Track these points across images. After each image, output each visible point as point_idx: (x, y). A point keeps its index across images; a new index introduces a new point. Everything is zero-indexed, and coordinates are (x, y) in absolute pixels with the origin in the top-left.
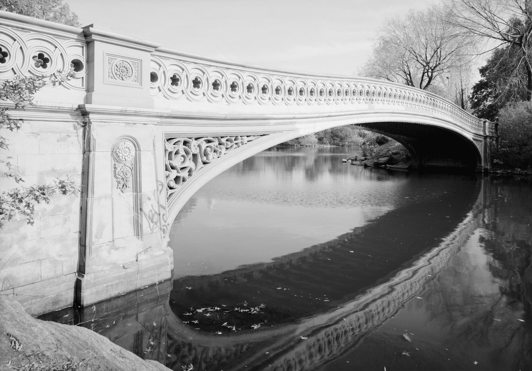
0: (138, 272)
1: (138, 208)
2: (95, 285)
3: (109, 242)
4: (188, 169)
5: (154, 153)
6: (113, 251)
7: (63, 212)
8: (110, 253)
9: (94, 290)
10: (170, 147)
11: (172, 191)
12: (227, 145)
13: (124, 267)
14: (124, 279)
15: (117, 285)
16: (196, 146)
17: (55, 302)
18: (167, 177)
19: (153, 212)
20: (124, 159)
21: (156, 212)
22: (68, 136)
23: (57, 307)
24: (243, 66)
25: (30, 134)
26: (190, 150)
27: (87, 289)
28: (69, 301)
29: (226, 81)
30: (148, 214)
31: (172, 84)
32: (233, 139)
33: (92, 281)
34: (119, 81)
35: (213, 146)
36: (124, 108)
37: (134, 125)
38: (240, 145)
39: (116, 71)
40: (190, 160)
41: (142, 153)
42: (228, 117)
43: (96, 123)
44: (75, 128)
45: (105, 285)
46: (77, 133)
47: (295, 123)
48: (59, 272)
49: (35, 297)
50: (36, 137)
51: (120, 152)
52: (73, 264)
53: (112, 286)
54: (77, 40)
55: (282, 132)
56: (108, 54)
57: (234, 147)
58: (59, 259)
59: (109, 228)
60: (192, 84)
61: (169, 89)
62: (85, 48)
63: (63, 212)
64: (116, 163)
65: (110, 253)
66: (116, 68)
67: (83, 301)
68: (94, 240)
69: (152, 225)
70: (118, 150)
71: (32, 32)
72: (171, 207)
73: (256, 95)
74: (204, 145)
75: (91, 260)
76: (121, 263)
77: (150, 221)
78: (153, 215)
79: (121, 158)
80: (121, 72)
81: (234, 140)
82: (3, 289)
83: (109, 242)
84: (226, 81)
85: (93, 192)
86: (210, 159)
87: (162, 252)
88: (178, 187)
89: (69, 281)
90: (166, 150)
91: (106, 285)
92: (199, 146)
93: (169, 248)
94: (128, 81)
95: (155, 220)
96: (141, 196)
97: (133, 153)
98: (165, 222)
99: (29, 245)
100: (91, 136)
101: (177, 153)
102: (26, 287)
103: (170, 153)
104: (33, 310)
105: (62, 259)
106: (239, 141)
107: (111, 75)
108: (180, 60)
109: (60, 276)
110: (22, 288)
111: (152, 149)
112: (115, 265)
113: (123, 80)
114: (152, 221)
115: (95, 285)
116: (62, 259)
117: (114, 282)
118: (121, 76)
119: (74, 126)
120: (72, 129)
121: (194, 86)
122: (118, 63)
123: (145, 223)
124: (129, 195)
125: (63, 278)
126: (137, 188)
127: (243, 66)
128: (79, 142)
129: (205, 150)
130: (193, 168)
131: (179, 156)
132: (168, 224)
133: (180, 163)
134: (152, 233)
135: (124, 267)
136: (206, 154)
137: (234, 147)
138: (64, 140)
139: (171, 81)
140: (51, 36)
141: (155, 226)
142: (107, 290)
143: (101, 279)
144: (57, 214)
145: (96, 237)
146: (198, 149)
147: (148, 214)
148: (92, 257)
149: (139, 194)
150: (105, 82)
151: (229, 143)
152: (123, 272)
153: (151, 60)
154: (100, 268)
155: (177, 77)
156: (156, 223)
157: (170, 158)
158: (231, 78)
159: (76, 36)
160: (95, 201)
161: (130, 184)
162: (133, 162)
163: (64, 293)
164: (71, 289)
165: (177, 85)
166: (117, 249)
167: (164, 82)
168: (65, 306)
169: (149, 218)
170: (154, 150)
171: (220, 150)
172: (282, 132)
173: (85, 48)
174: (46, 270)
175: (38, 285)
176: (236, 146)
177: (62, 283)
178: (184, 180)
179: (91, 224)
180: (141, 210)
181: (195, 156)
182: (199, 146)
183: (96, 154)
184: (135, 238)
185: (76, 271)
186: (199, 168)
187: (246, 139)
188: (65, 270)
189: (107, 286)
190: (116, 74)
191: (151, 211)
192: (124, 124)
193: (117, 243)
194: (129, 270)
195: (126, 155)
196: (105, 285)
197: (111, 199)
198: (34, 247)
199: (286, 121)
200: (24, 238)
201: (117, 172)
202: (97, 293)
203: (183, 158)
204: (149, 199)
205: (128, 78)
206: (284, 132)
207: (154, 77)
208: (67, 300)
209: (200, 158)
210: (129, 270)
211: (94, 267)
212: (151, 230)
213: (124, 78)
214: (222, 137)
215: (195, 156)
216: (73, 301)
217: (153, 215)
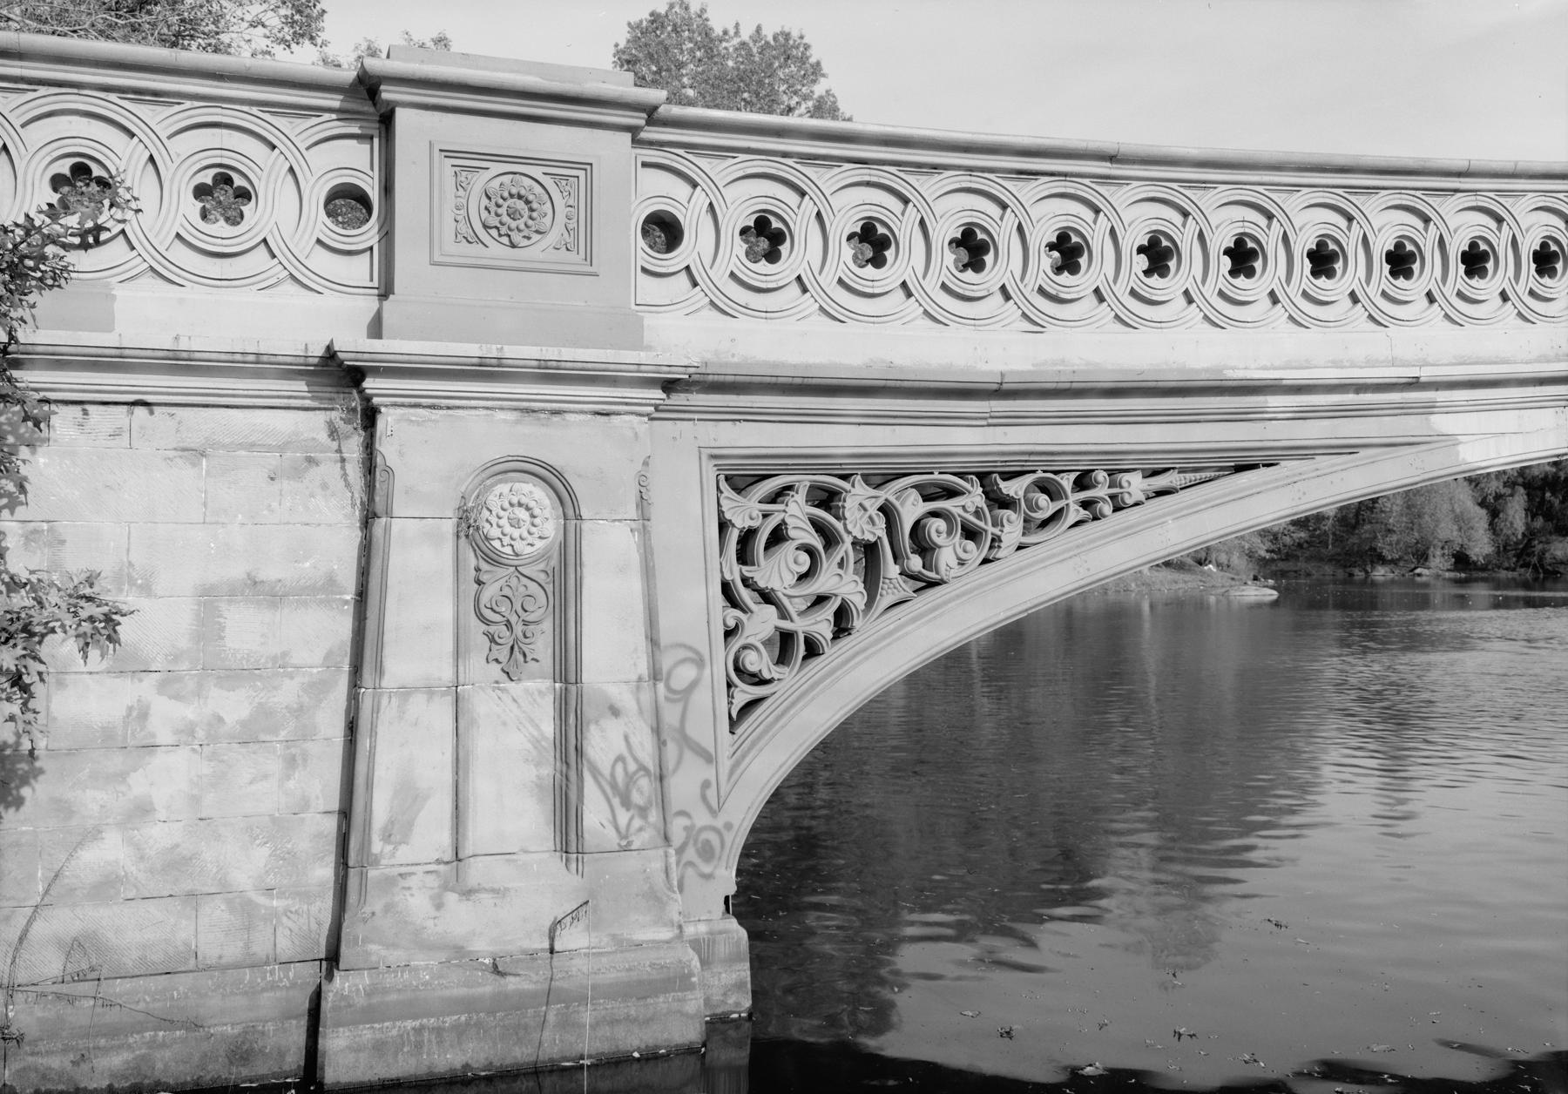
0: (549, 996)
1: (569, 749)
2: (370, 1014)
3: (438, 862)
4: (833, 606)
5: (645, 532)
6: (451, 898)
7: (283, 735)
8: (439, 906)
9: (367, 1034)
10: (745, 511)
11: (759, 691)
12: (1032, 506)
13: (495, 966)
14: (491, 1012)
15: (460, 1031)
16: (873, 511)
17: (241, 1052)
18: (729, 634)
19: (632, 767)
20: (508, 550)
21: (642, 768)
22: (310, 460)
23: (245, 1072)
24: (1112, 158)
25: (172, 454)
26: (839, 525)
27: (338, 1025)
28: (289, 1059)
29: (1441, 241)
30: (606, 772)
31: (1231, 272)
32: (1067, 481)
33: (360, 1001)
34: (497, 250)
35: (957, 511)
36: (491, 351)
37: (556, 419)
38: (1107, 508)
39: (484, 214)
40: (841, 565)
41: (586, 526)
42: (1011, 383)
43: (400, 411)
44: (333, 433)
45: (410, 1024)
46: (339, 451)
47: (1429, 409)
48: (261, 948)
49: (167, 1023)
50: (194, 465)
51: (494, 520)
52: (314, 926)
53: (439, 1031)
54: (344, 114)
55: (1350, 449)
56: (448, 153)
57: (1072, 517)
58: (261, 900)
59: (441, 804)
60: (1308, 265)
61: (944, 287)
62: (376, 141)
63: (283, 735)
64: (484, 566)
65: (439, 906)
66: (485, 201)
67: (322, 1069)
68: (377, 846)
69: (623, 817)
70: (486, 513)
71: (188, 104)
72: (744, 756)
73: (1356, 286)
74: (911, 509)
75: (365, 921)
76: (482, 946)
77: (616, 801)
78: (630, 779)
79: (496, 544)
80: (511, 216)
81: (1085, 488)
82: (68, 978)
83: (438, 862)
84: (1441, 241)
85: (380, 670)
86: (942, 567)
87: (666, 934)
88: (788, 679)
89: (293, 985)
90: (723, 526)
91: (417, 1023)
92: (887, 510)
93: (733, 923)
94: (538, 250)
95: (637, 798)
96: (580, 695)
97: (550, 527)
98: (714, 813)
99: (159, 835)
100: (379, 460)
101: (778, 537)
102: (141, 981)
103: (748, 536)
104: (159, 1065)
105: (275, 903)
106: (1101, 492)
107: (464, 229)
108: (785, 155)
109: (267, 963)
110: (128, 985)
111: (632, 512)
112: (459, 954)
113: (513, 246)
114: (627, 803)
115: (370, 1014)
116: (275, 903)
117: (449, 1020)
118: (504, 230)
119: (330, 424)
120: (323, 436)
121: (1316, 273)
122: (496, 183)
123: (595, 813)
124: (535, 696)
125: (272, 973)
126: (567, 670)
127: (1112, 158)
128: (348, 485)
129: (917, 527)
130: (858, 599)
131: (787, 550)
132: (728, 826)
133: (791, 579)
134: (626, 849)
135: (495, 966)
136: (924, 548)
137: (1072, 517)
138: (296, 473)
139: (1227, 262)
140: (255, 110)
141: (637, 823)
142: (419, 1046)
143: (393, 997)
144: (262, 737)
145: (387, 837)
146: (881, 522)
147: (606, 772)
148: (367, 909)
149: (573, 688)
150: (437, 258)
151: (1043, 499)
152: (488, 987)
153: (645, 165)
154: (396, 956)
155: (1409, 247)
156: (643, 811)
157: (744, 557)
158: (1463, 228)
159: (335, 101)
160: (385, 701)
161: (542, 646)
162: (554, 562)
163: (270, 1027)
164: (296, 1017)
165: (1250, 273)
166: (468, 893)
167: (711, 246)
168: (274, 1075)
169: (614, 786)
170: (645, 518)
171: (991, 529)
172: (1350, 449)
173: (376, 141)
174: (212, 934)
175: (183, 983)
176: (1083, 514)
177: (264, 990)
178: (813, 650)
179: (369, 786)
180: (579, 751)
181: (869, 551)
182: (887, 510)
183: (396, 525)
184: (556, 863)
185: (323, 956)
186: (884, 600)
187: (1135, 485)
188: (286, 946)
189: (419, 1031)
190: (486, 227)
191: (620, 759)
192: (511, 416)
193: (476, 872)
194: (511, 984)
195: (516, 533)
196: (410, 1024)
197: (450, 699)
198: (177, 846)
199: (1350, 398)
200: (143, 810)
201: (484, 599)
202: (379, 1047)
203: (805, 559)
204: (615, 712)
205: (536, 237)
206: (1363, 452)
207: (665, 230)
208: (281, 1054)
209: (903, 557)
210: (511, 984)
211: (373, 947)
212: (623, 837)
213: (516, 237)
214: (1009, 476)
215: (869, 551)
216: (302, 1063)
217: (630, 779)
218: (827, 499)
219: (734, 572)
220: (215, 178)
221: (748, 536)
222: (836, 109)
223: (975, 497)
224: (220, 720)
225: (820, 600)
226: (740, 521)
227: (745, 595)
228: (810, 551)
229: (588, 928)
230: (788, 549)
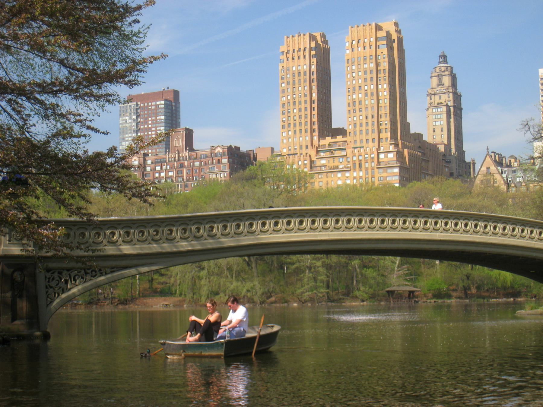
18: (47, 292)
62: (158, 103)
90: (46, 277)
101: (53, 279)
103: (49, 279)
203: (57, 282)
214: (88, 269)
218: (60, 273)
219: (47, 284)
220: (34, 50)
221: (49, 279)
222: (443, 84)
223: (83, 272)
224: (116, 150)
225: (60, 288)
226: (48, 277)
227: (48, 287)
228: (58, 280)
229: (491, 277)
230: (55, 280)
